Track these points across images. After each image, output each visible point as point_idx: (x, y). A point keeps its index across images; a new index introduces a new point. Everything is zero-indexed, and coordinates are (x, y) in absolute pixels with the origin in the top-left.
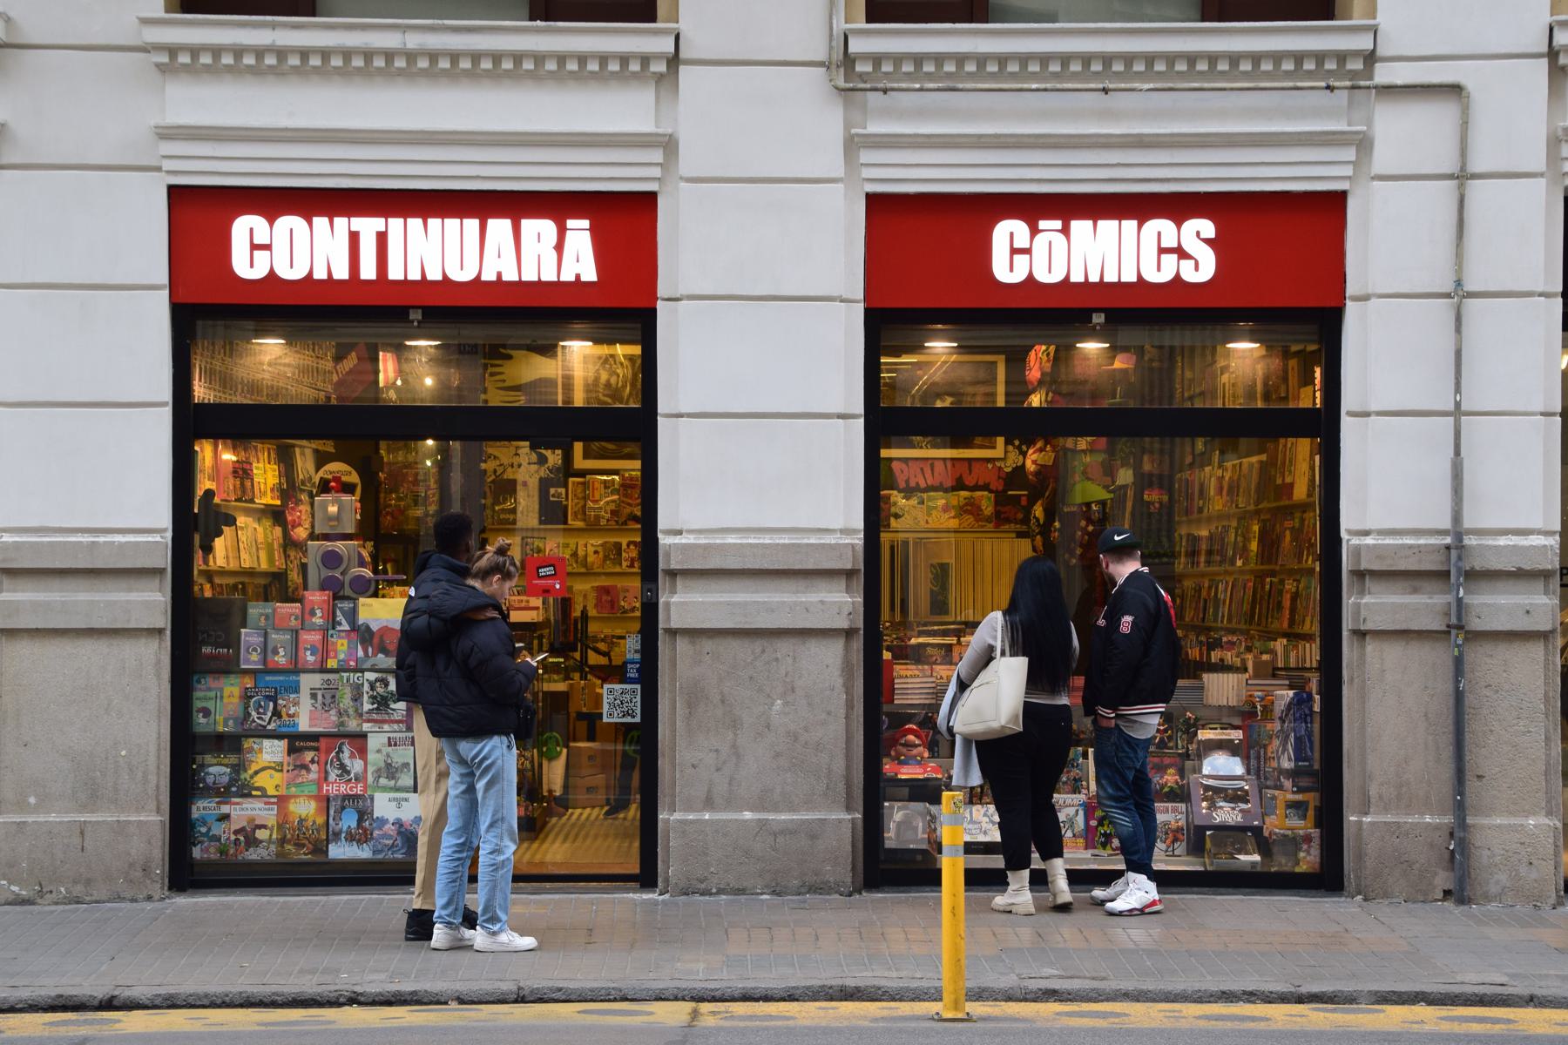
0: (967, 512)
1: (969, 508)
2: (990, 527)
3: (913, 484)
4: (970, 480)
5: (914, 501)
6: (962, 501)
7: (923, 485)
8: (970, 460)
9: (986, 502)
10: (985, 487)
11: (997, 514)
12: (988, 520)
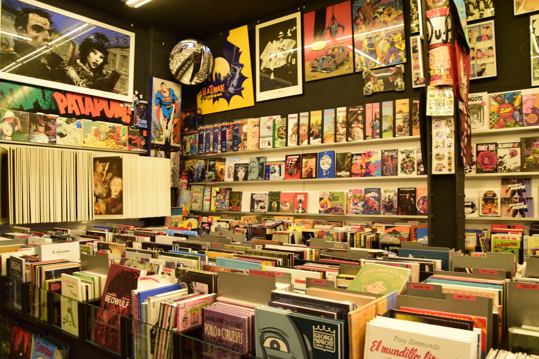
0: (110, 137)
1: (112, 135)
2: (126, 148)
3: (70, 112)
4: (109, 115)
5: (73, 125)
6: (108, 130)
7: (78, 113)
8: (109, 100)
9: (123, 130)
10: (118, 120)
11: (130, 140)
12: (124, 145)
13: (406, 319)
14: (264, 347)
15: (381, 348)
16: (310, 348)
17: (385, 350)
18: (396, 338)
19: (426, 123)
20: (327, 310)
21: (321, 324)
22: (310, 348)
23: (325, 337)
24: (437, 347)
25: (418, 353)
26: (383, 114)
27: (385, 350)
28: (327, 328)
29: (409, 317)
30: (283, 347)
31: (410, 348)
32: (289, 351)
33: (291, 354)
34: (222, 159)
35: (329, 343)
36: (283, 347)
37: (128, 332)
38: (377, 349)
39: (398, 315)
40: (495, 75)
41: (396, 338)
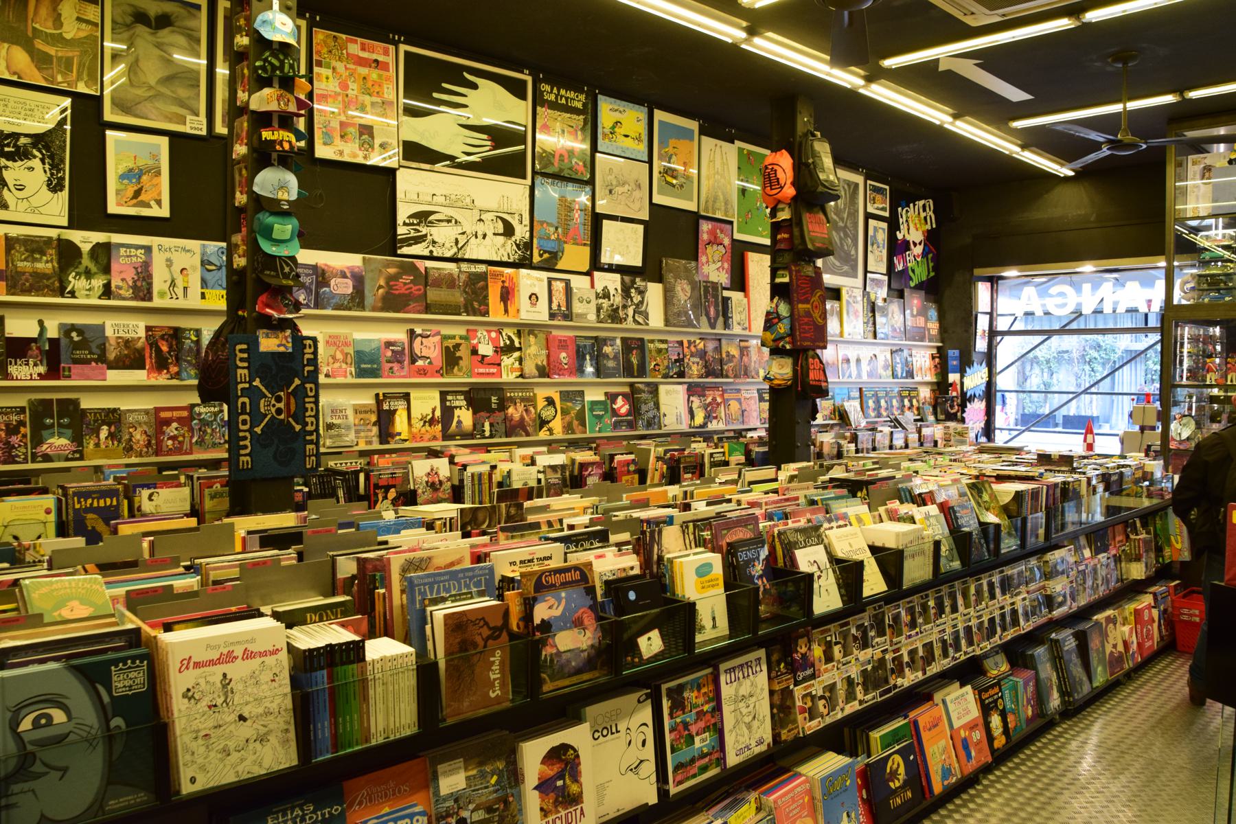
13: (186, 628)
14: (18, 734)
15: (191, 664)
16: (106, 699)
17: (197, 665)
18: (208, 646)
19: (991, 315)
20: (108, 643)
21: (124, 660)
22: (106, 699)
23: (131, 675)
24: (253, 641)
25: (235, 654)
26: (587, 250)
27: (197, 665)
28: (133, 662)
29: (182, 625)
30: (59, 716)
31: (225, 651)
32: (70, 717)
33: (74, 721)
34: (235, 82)
35: (137, 681)
36: (59, 716)
37: (578, 671)
38: (187, 668)
39: (176, 627)
40: (640, 264)
41: (208, 646)
